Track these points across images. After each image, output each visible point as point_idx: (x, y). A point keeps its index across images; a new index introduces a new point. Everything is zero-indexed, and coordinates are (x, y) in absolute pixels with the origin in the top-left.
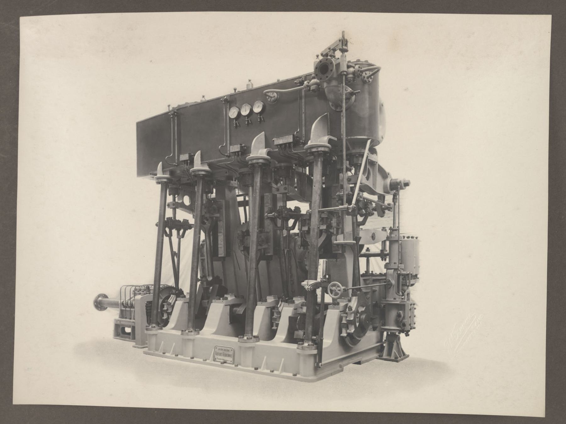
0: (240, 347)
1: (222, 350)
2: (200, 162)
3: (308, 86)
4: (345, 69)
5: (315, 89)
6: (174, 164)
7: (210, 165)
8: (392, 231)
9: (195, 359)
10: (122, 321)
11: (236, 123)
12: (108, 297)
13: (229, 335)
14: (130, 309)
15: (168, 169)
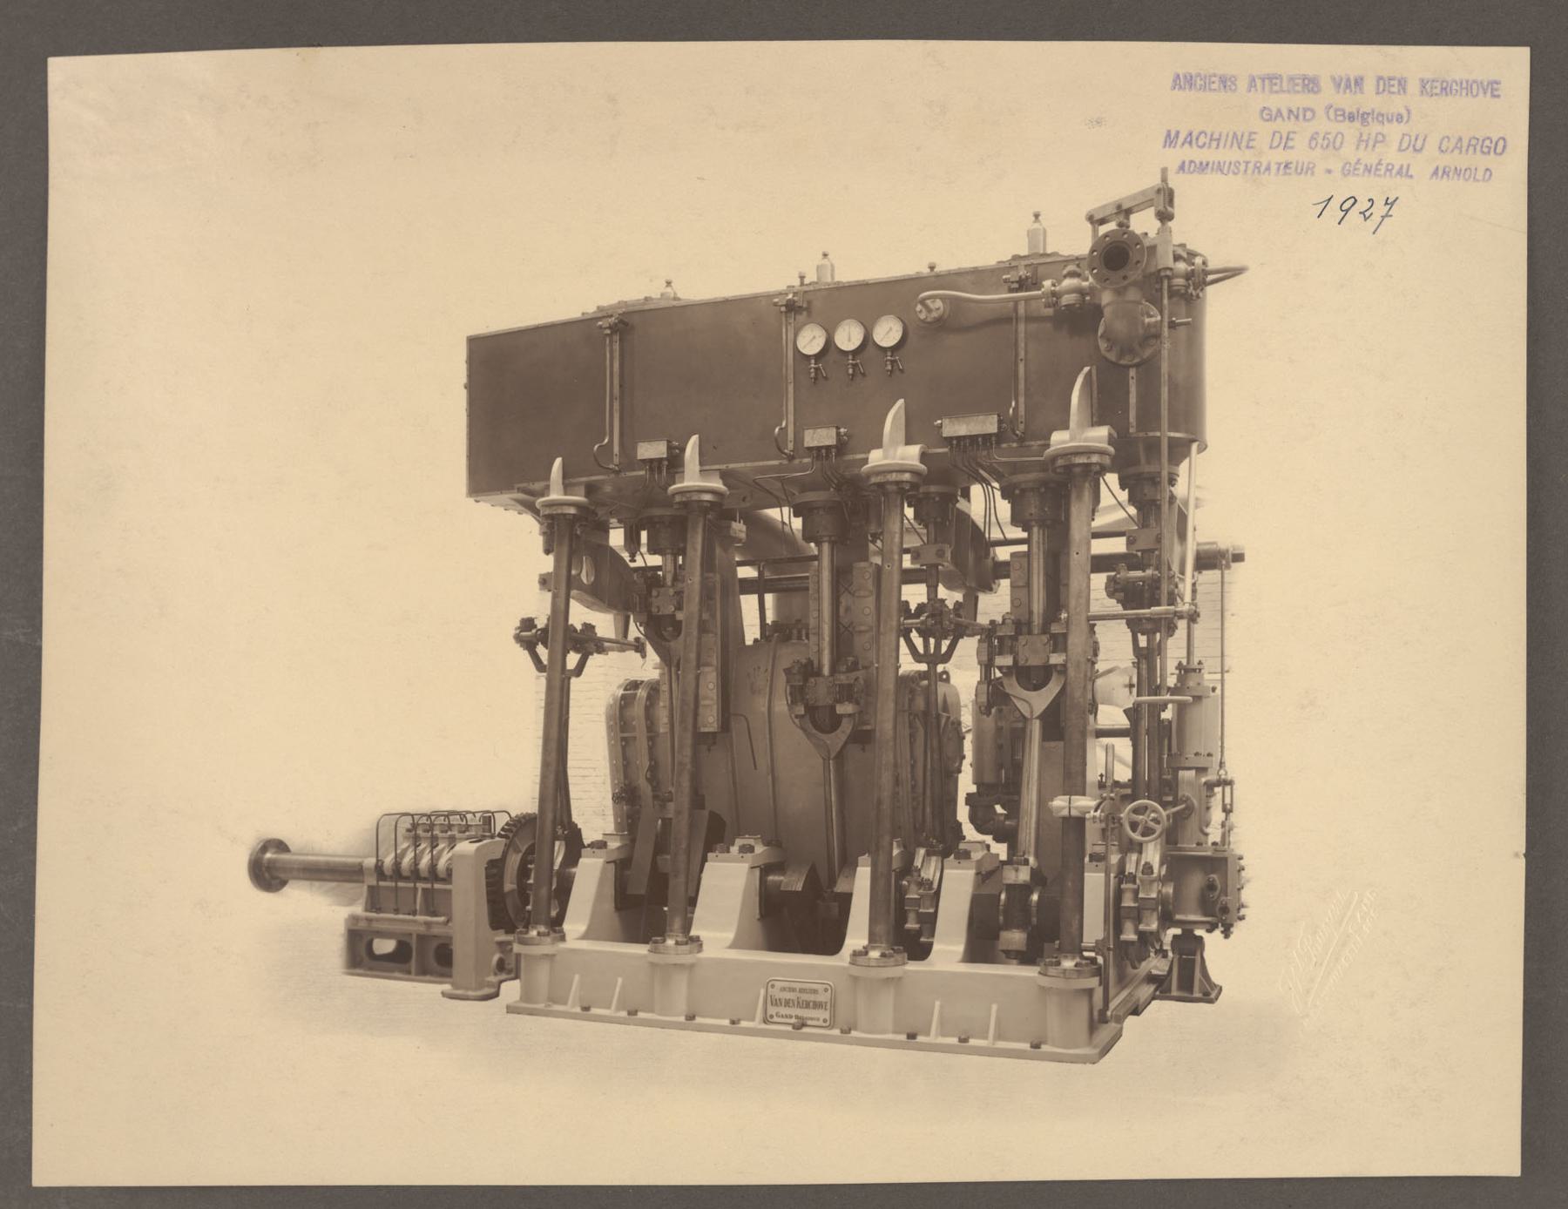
0: (855, 979)
1: (793, 990)
2: (698, 468)
3: (1054, 294)
4: (1170, 263)
5: (1074, 304)
6: (611, 466)
7: (725, 476)
8: (1183, 672)
9: (699, 1020)
10: (377, 920)
11: (817, 369)
12: (290, 847)
13: (757, 948)
14: (378, 884)
15: (584, 479)
